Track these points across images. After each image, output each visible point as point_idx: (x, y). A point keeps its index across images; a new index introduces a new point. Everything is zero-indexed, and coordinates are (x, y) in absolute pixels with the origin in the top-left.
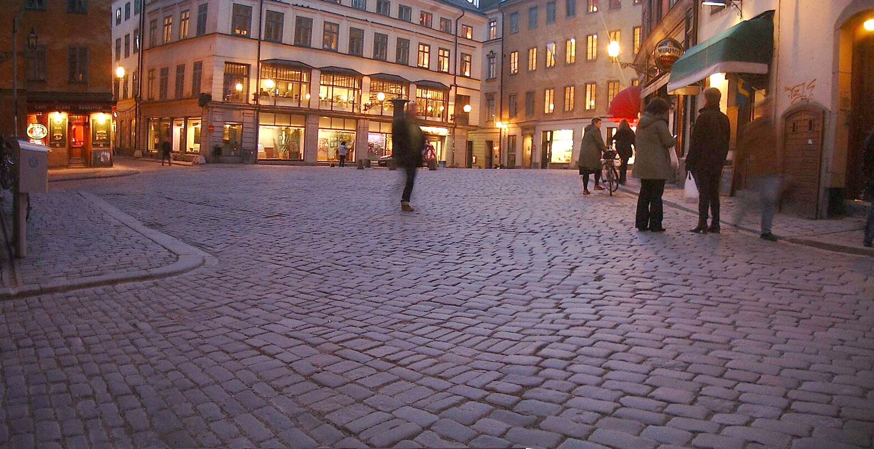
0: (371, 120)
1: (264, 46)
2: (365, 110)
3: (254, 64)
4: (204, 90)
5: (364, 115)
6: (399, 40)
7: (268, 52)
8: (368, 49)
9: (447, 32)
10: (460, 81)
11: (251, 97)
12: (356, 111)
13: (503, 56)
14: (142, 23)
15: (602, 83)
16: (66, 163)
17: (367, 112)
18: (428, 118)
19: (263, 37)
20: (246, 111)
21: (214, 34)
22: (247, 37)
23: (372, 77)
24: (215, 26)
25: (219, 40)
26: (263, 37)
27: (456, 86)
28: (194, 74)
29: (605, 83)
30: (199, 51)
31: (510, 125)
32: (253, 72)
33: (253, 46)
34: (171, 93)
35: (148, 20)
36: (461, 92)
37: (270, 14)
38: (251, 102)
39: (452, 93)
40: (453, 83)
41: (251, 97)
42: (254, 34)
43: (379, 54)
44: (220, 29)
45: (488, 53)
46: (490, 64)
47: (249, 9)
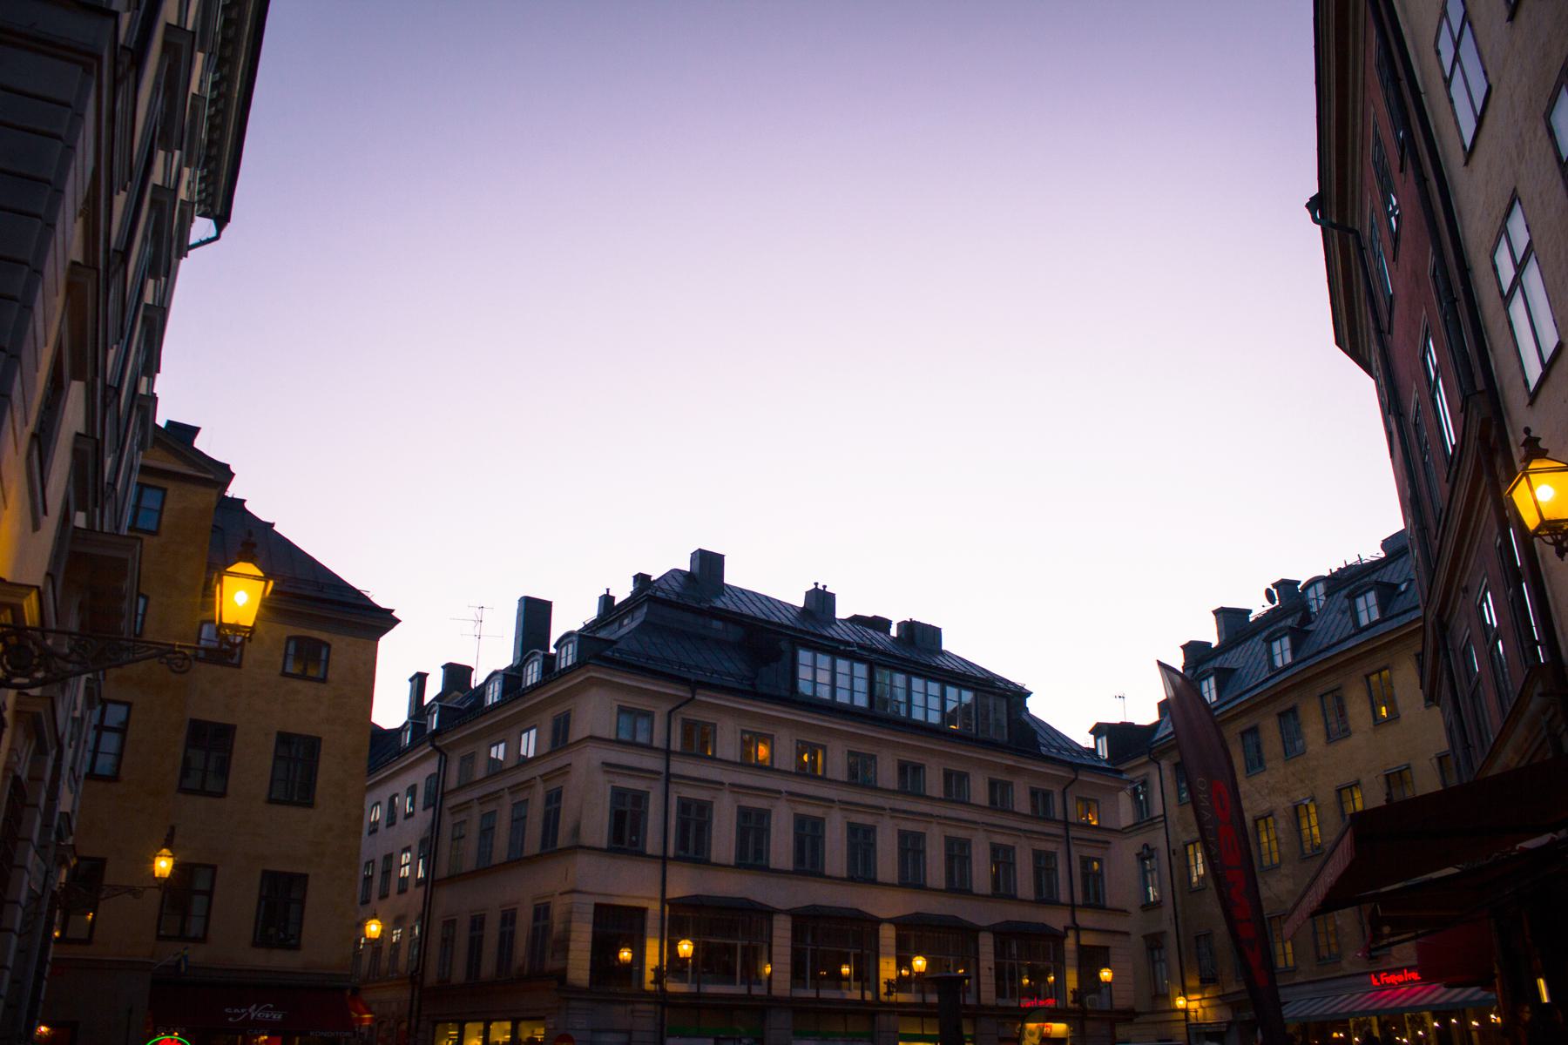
0: (902, 1014)
2: (889, 993)
3: (654, 907)
4: (551, 964)
5: (888, 1004)
6: (950, 842)
7: (682, 883)
8: (887, 864)
9: (1048, 819)
10: (1085, 918)
11: (649, 976)
12: (869, 996)
13: (1171, 853)
14: (436, 826)
15: (1327, 795)
16: (112, 22)
17: (892, 998)
18: (1025, 1003)
19: (1079, 899)
20: (638, 1007)
21: (577, 848)
22: (641, 854)
23: (900, 923)
24: (576, 831)
25: (583, 862)
26: (671, 852)
27: (1077, 929)
28: (535, 929)
29: (1332, 797)
30: (547, 882)
31: (1204, 1003)
32: (652, 923)
34: (488, 967)
35: (448, 821)
36: (1088, 939)
37: (685, 805)
38: (649, 986)
39: (1070, 943)
40: (1068, 922)
41: (649, 976)
42: (653, 845)
43: (912, 880)
44: (586, 840)
45: (1139, 849)
46: (1144, 873)
47: (640, 798)
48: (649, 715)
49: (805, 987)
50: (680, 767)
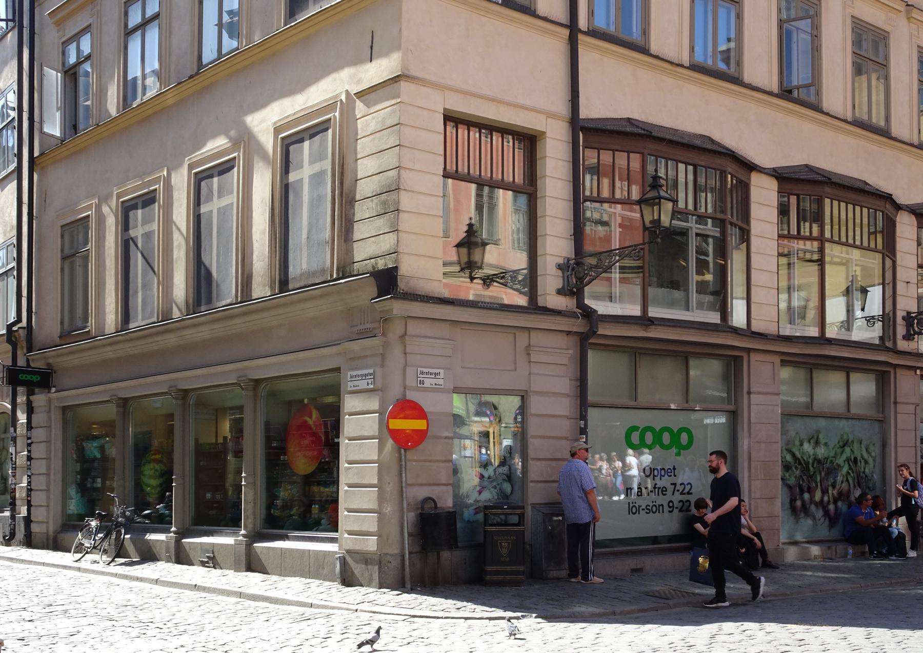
1: (591, 55)
2: (908, 337)
33: (550, 49)
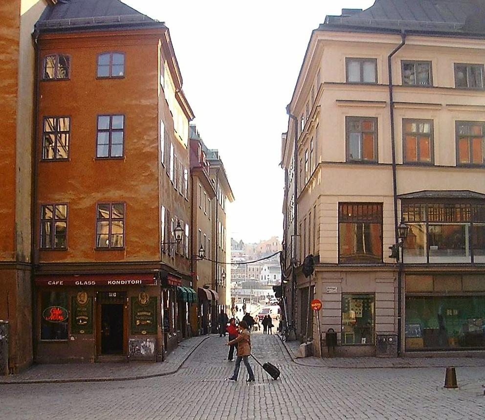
1: (402, 174)
26: (399, 160)
33: (385, 175)
42: (384, 156)
48: (374, 61)
49: (464, 254)
50: (400, 96)
